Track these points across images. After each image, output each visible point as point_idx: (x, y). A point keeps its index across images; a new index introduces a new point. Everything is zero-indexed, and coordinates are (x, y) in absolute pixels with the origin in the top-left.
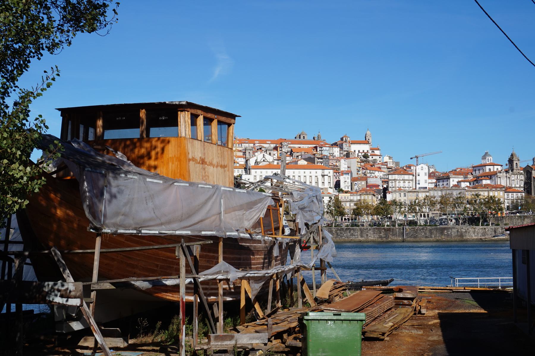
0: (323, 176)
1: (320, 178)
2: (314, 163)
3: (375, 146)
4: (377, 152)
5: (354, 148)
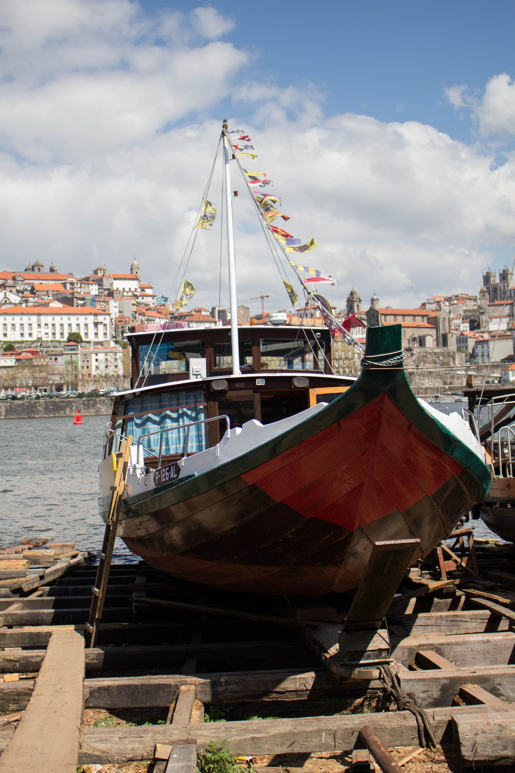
0: (96, 324)
1: (91, 327)
2: (73, 306)
3: (144, 283)
4: (148, 291)
5: (118, 285)
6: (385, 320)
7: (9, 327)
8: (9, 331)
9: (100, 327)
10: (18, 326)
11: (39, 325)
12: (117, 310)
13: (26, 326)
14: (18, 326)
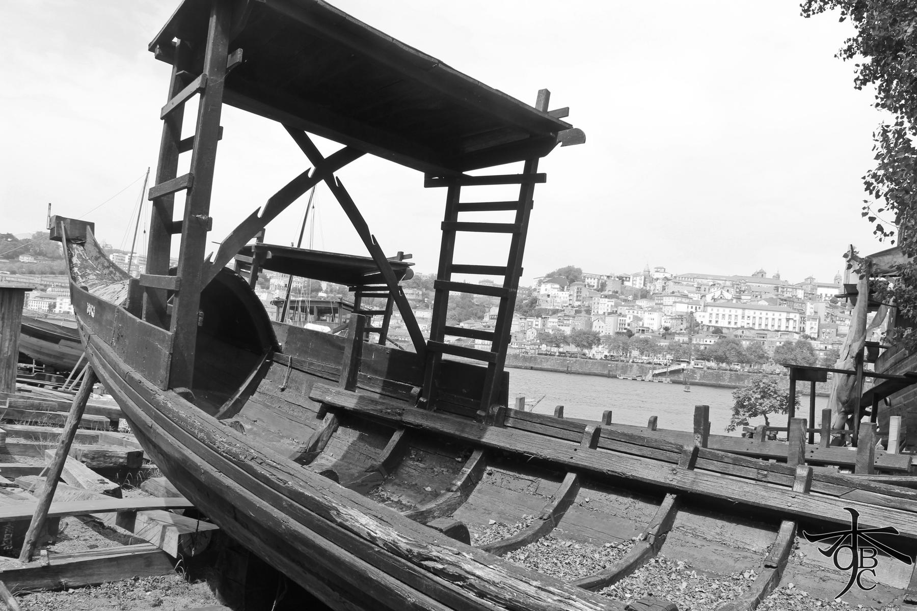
0: (788, 320)
6: (702, 415)
7: (720, 316)
8: (720, 320)
9: (791, 322)
10: (727, 317)
11: (743, 317)
12: (812, 311)
13: (733, 317)
14: (727, 317)
